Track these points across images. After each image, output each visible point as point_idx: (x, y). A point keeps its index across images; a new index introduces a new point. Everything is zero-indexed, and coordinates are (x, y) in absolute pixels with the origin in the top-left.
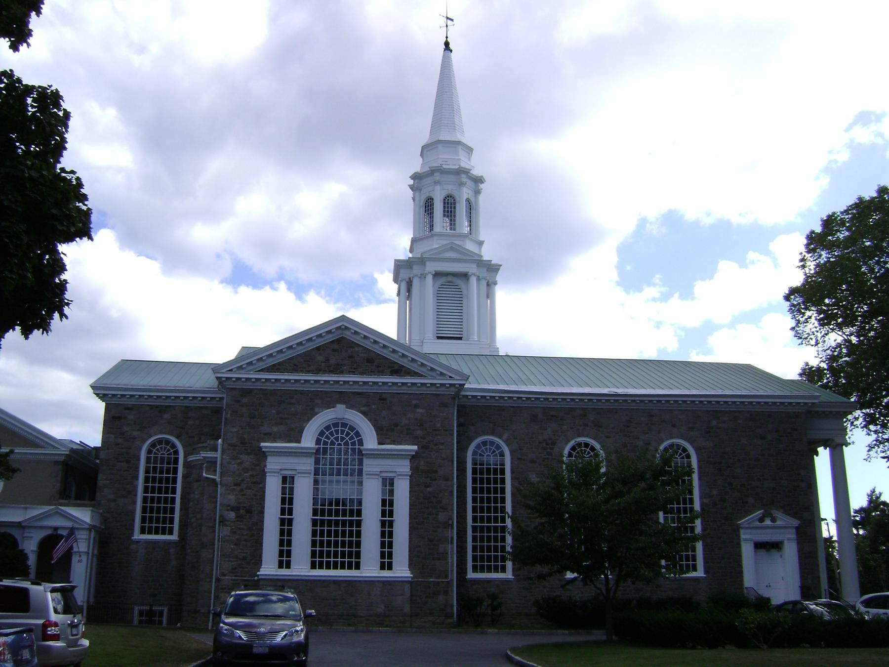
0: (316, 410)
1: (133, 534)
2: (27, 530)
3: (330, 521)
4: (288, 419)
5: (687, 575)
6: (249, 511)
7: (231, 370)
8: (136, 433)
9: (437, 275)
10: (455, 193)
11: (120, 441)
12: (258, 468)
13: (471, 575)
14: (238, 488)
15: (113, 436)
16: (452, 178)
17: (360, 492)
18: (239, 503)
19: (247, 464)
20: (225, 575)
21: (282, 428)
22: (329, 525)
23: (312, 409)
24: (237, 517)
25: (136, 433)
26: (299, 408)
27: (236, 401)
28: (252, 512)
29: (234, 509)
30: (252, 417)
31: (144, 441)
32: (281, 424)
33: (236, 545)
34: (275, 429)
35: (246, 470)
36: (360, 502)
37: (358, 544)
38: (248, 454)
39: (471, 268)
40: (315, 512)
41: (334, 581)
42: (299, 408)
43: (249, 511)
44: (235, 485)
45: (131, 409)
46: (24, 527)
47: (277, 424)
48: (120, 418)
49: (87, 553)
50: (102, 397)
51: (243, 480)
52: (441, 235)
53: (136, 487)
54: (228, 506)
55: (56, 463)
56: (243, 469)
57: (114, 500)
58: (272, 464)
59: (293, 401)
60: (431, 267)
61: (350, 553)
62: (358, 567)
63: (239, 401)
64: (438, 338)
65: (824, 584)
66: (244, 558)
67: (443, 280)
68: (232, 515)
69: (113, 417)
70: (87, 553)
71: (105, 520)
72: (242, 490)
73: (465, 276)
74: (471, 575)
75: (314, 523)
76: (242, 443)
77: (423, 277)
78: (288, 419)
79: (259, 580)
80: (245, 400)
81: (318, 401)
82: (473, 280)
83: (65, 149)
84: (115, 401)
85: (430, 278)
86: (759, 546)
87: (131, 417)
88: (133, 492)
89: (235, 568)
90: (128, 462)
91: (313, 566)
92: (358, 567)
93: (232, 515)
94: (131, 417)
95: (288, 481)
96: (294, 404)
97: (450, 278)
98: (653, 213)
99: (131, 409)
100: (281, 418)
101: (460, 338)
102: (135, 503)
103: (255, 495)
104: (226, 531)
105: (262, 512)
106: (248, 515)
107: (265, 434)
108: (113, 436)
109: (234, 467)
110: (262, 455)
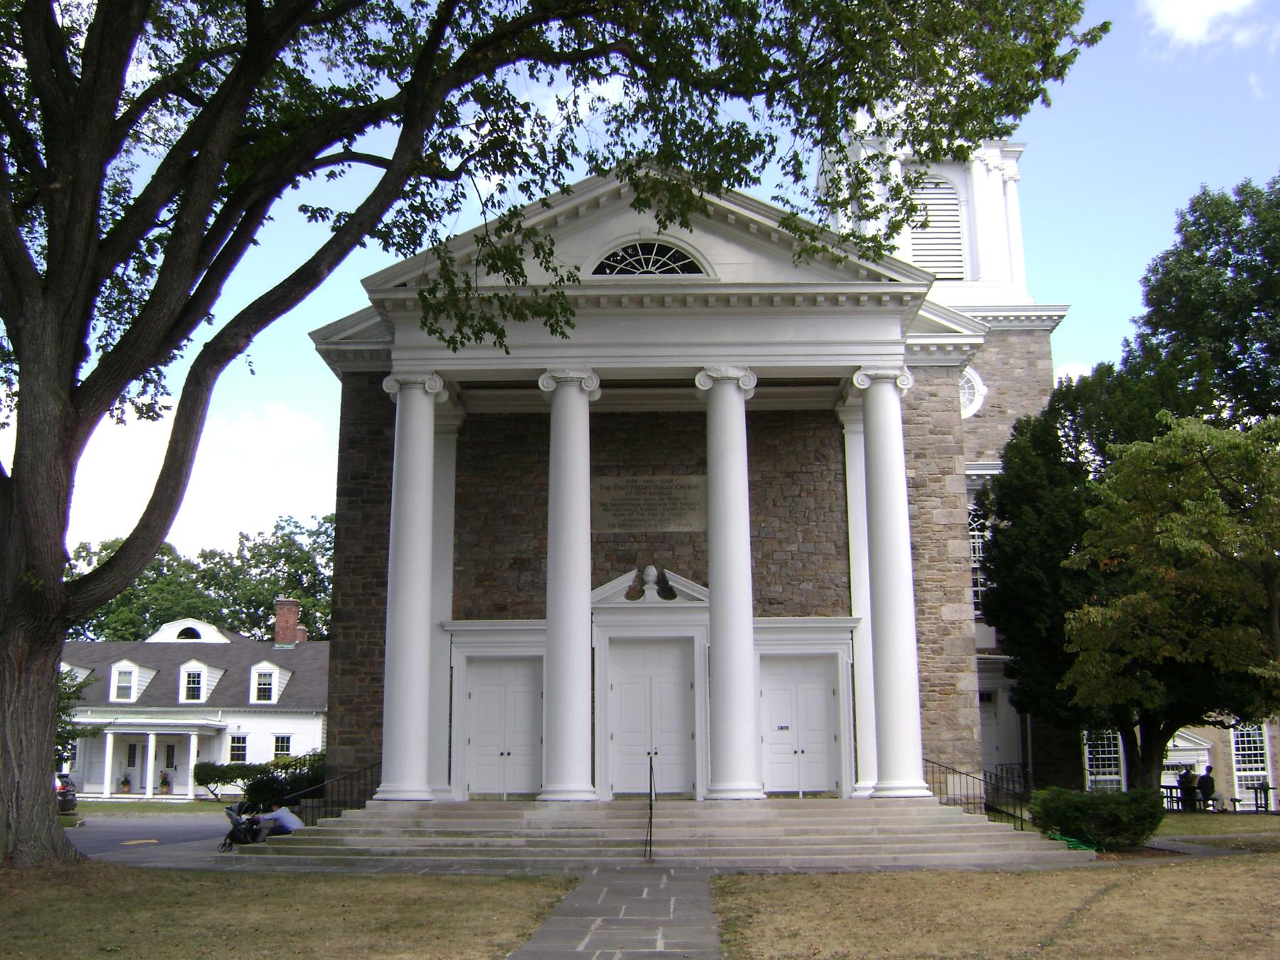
5: (1086, 749)
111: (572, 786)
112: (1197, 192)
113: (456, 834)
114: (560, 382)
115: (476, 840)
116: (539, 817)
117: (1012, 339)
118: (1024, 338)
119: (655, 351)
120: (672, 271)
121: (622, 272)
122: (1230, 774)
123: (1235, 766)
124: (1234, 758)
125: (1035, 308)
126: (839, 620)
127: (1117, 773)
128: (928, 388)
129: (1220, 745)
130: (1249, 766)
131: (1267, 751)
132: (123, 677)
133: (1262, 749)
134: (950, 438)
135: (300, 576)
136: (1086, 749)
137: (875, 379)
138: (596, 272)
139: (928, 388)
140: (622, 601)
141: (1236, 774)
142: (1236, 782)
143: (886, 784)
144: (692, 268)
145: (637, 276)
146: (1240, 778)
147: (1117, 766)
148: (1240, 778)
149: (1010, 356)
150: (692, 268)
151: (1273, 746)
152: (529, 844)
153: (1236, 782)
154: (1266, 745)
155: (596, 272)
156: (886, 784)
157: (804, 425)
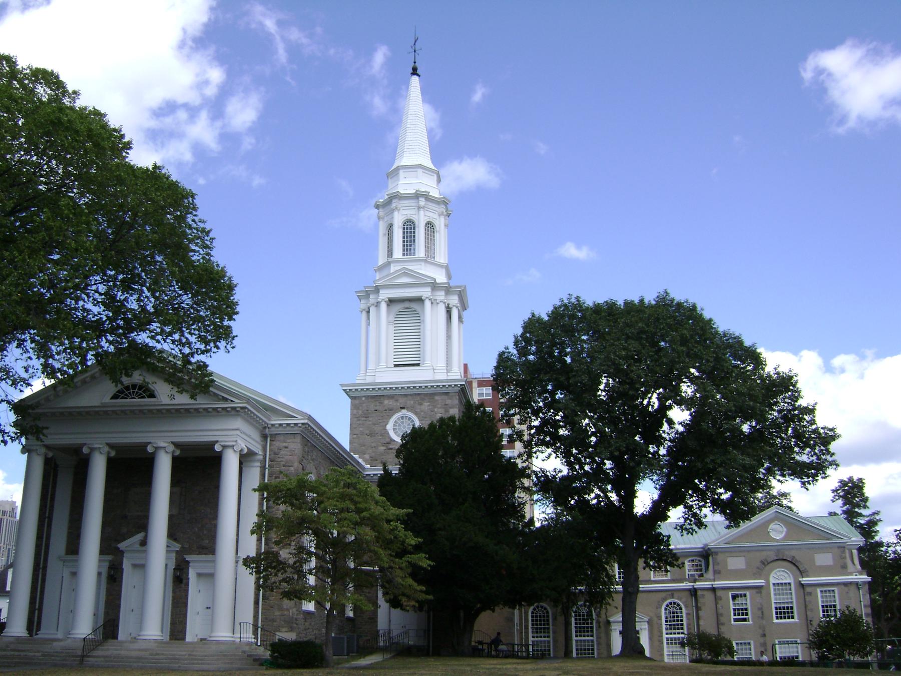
5: (573, 620)
9: (391, 302)
10: (415, 218)
13: (818, 590)
16: (412, 203)
39: (425, 292)
52: (398, 261)
60: (385, 294)
64: (396, 366)
67: (397, 308)
73: (419, 300)
74: (818, 590)
77: (378, 305)
82: (428, 304)
83: (636, 497)
85: (384, 306)
86: (199, 575)
97: (407, 304)
98: (691, 301)
101: (418, 365)
111: (81, 632)
112: (527, 316)
113: (19, 651)
114: (92, 450)
115: (22, 654)
116: (136, 646)
117: (437, 398)
118: (445, 397)
119: (132, 435)
120: (143, 397)
121: (123, 398)
122: (661, 636)
123: (664, 631)
124: (664, 627)
125: (447, 381)
126: (210, 557)
127: (592, 636)
128: (284, 444)
129: (655, 619)
130: (673, 631)
131: (685, 622)
132: (142, 562)
133: (682, 621)
134: (292, 468)
135: (594, 447)
136: (573, 620)
137: (224, 447)
138: (112, 398)
139: (284, 444)
140: (137, 547)
141: (665, 636)
142: (665, 641)
143: (213, 635)
144: (152, 396)
145: (128, 400)
146: (667, 639)
147: (592, 631)
148: (667, 639)
149: (435, 407)
150: (152, 396)
151: (688, 619)
152: (43, 655)
153: (665, 641)
154: (684, 619)
155: (112, 398)
156: (213, 635)
157: (199, 469)
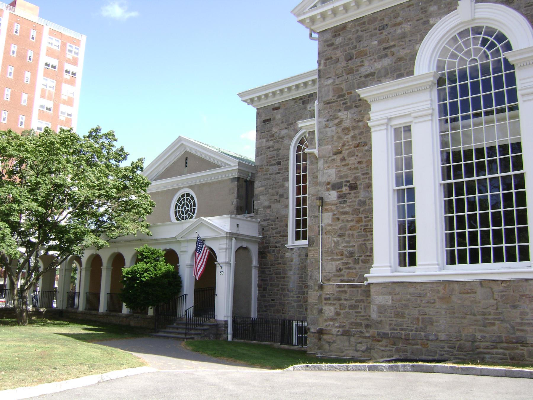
0: (431, 22)
1: (286, 241)
2: (183, 244)
3: (471, 185)
4: (394, 46)
6: (353, 187)
7: (315, 6)
8: (284, 132)
11: (271, 143)
12: (361, 124)
14: (338, 157)
15: (264, 140)
17: (516, 130)
18: (341, 177)
19: (347, 123)
20: (329, 280)
21: (386, 62)
22: (471, 191)
23: (426, 22)
24: (339, 197)
25: (284, 132)
26: (407, 27)
27: (328, 46)
28: (356, 187)
29: (336, 187)
30: (349, 58)
31: (291, 138)
32: (386, 56)
33: (340, 236)
34: (378, 65)
35: (346, 130)
36: (517, 147)
37: (523, 217)
38: (346, 109)
40: (446, 173)
41: (481, 282)
42: (407, 27)
43: (353, 187)
44: (335, 154)
45: (278, 108)
46: (179, 242)
47: (380, 58)
48: (269, 120)
49: (229, 264)
50: (251, 101)
51: (344, 145)
53: (287, 189)
54: (328, 184)
55: (233, 179)
56: (344, 129)
57: (269, 207)
58: (377, 114)
59: (399, 20)
61: (510, 233)
62: (525, 256)
63: (332, 44)
65: (493, 321)
66: (351, 254)
68: (332, 196)
69: (265, 121)
70: (229, 264)
71: (263, 229)
72: (343, 159)
75: (448, 190)
76: (339, 96)
78: (394, 46)
79: (369, 284)
80: (338, 40)
81: (433, 8)
84: (264, 103)
87: (278, 117)
88: (284, 196)
89: (340, 270)
90: (279, 163)
91: (451, 261)
92: (525, 256)
93: (332, 196)
94: (278, 117)
95: (403, 133)
96: (400, 24)
99: (278, 108)
100: (385, 49)
102: (287, 206)
103: (359, 163)
104: (326, 218)
105: (369, 186)
106: (353, 192)
107: (367, 76)
108: (264, 140)
109: (332, 131)
110: (362, 107)
